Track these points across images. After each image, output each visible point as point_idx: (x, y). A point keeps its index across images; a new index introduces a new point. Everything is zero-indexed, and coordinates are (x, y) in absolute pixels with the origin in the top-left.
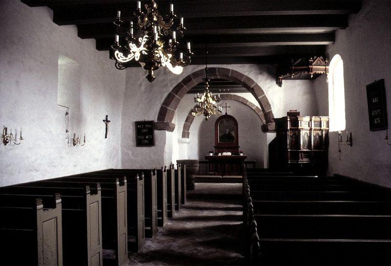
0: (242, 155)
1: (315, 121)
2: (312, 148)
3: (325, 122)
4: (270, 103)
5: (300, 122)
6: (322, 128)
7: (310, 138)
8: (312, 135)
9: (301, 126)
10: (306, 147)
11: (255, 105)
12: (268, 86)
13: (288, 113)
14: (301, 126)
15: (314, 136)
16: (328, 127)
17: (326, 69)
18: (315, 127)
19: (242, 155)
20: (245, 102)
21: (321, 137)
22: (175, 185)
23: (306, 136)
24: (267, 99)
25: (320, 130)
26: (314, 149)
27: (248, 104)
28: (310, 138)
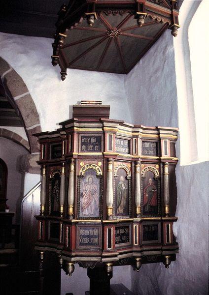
0: (7, 211)
1: (144, 141)
2: (138, 211)
3: (168, 142)
4: (39, 110)
5: (107, 136)
6: (164, 156)
7: (132, 183)
8: (138, 176)
9: (110, 149)
10: (121, 210)
11: (21, 138)
12: (36, 76)
13: (75, 109)
14: (110, 149)
15: (143, 179)
16: (175, 156)
17: (172, 15)
18: (143, 154)
19: (7, 211)
20: (17, 140)
21: (158, 182)
22: (65, 194)
23: (122, 178)
24: (32, 102)
25: (159, 162)
26: (144, 213)
27: (21, 142)
28: (132, 183)
